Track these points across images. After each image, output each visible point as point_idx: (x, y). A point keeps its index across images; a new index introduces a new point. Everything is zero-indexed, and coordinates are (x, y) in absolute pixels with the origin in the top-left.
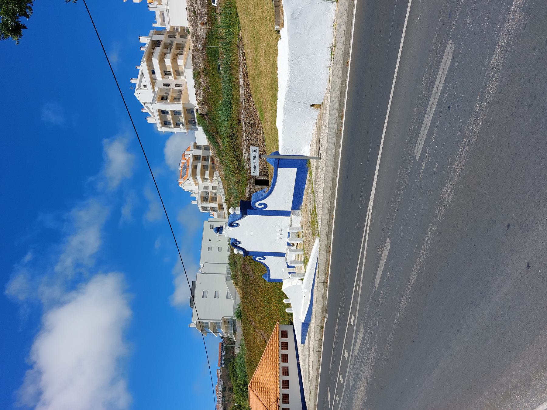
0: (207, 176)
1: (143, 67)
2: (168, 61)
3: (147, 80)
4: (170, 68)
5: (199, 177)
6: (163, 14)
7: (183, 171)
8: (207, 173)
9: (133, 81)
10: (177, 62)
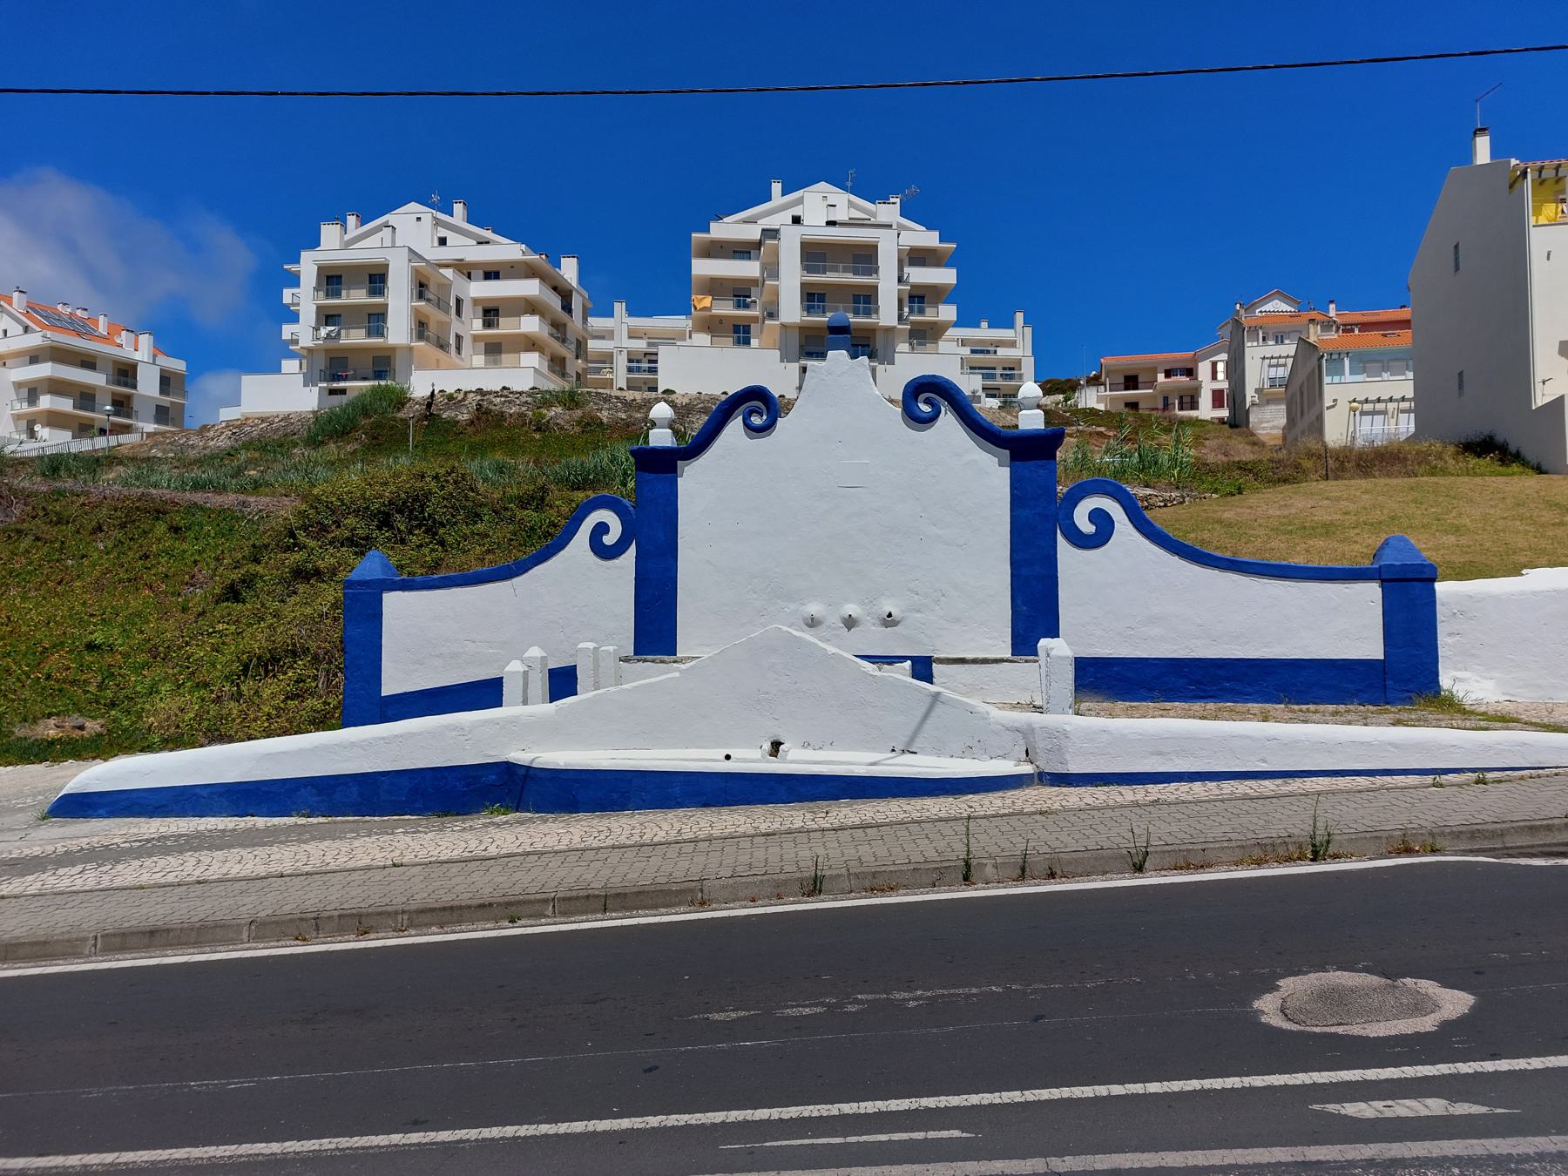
0: (46, 402)
1: (508, 250)
2: (531, 325)
3: (464, 248)
4: (507, 327)
5: (45, 370)
6: (603, 338)
7: (59, 317)
8: (66, 405)
9: (459, 208)
10: (527, 350)
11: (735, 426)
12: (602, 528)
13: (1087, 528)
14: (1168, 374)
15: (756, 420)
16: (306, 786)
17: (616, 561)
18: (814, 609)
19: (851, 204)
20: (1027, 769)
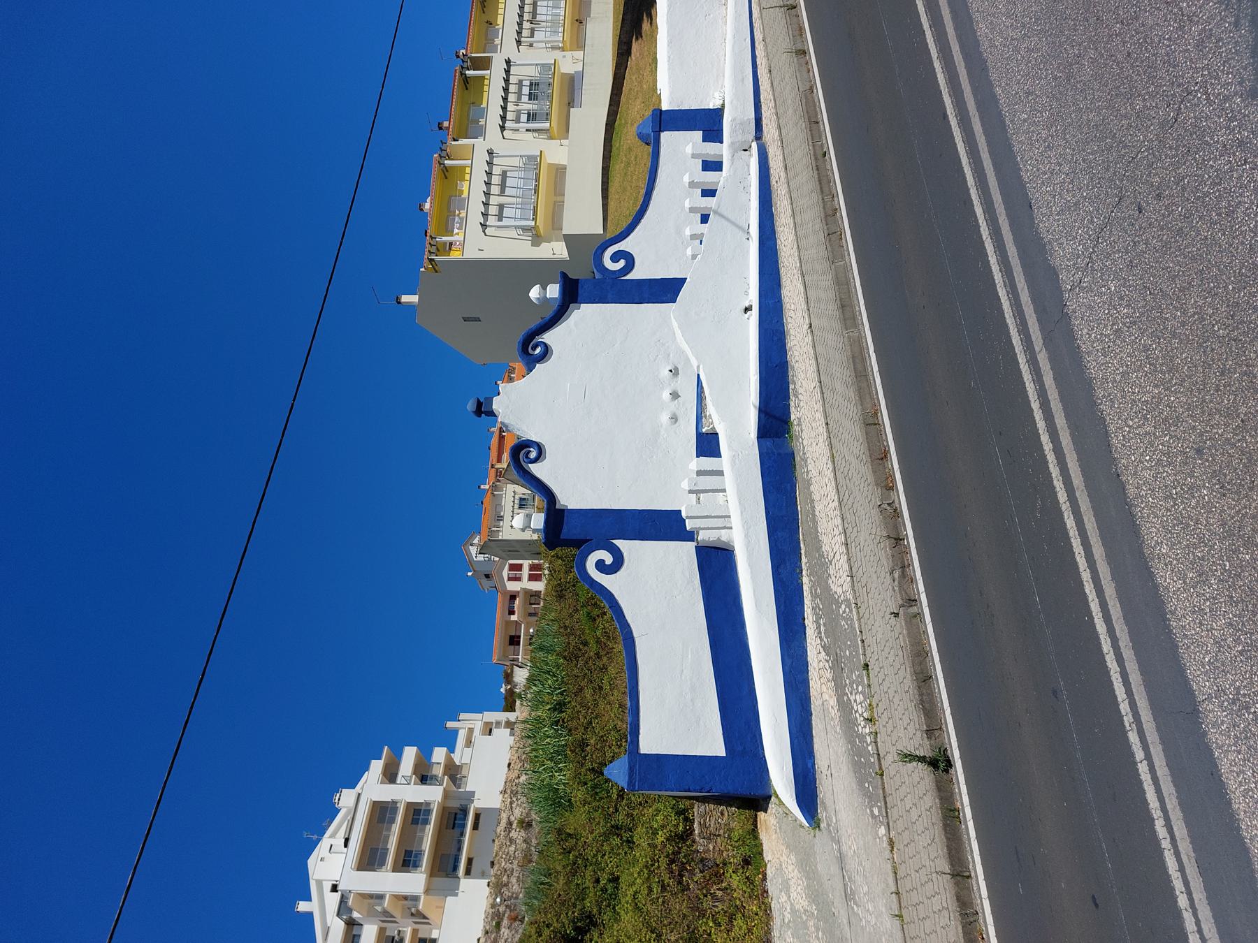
11: (535, 469)
12: (600, 565)
13: (622, 263)
14: (512, 612)
15: (533, 455)
16: (779, 574)
17: (625, 555)
18: (665, 418)
19: (333, 836)
20: (754, 145)
